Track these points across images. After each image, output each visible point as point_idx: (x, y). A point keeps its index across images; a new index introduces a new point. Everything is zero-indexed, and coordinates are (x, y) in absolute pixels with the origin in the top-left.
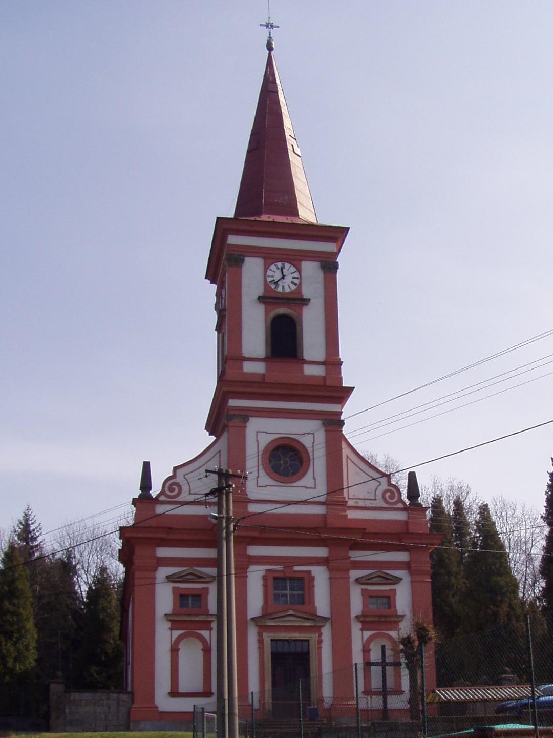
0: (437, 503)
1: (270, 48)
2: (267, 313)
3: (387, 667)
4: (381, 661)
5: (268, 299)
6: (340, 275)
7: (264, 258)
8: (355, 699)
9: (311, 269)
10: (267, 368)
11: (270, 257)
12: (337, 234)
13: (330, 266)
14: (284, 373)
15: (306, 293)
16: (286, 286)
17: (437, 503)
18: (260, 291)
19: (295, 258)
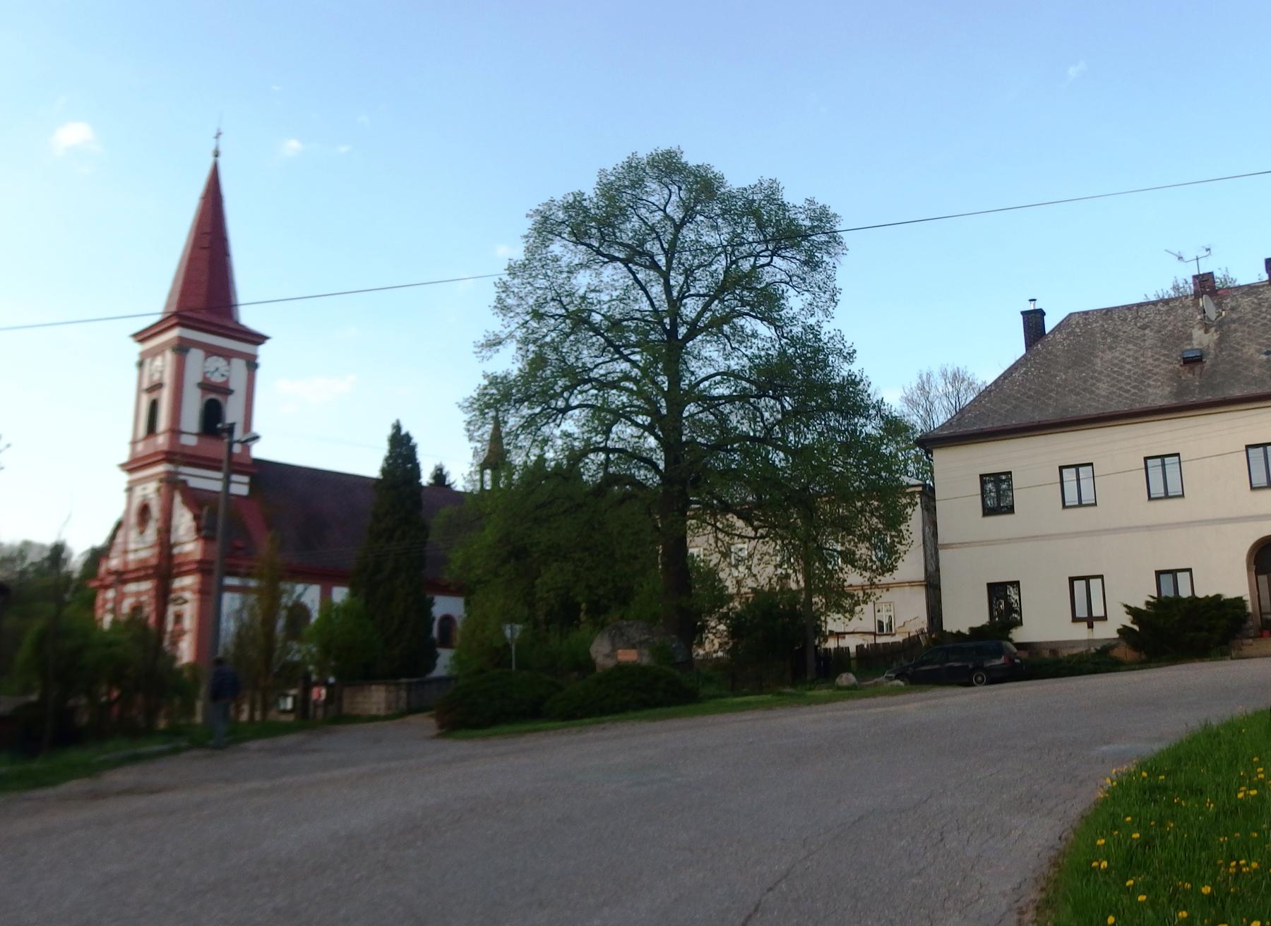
0: (1148, 603)
1: (217, 154)
2: (202, 397)
3: (1086, 615)
4: (1086, 615)
5: (206, 386)
6: (260, 374)
7: (205, 351)
8: (880, 633)
9: (239, 365)
10: (199, 441)
11: (211, 351)
12: (259, 339)
13: (252, 364)
14: (216, 449)
15: (232, 386)
16: (217, 379)
17: (1148, 603)
18: (199, 379)
19: (228, 355)
